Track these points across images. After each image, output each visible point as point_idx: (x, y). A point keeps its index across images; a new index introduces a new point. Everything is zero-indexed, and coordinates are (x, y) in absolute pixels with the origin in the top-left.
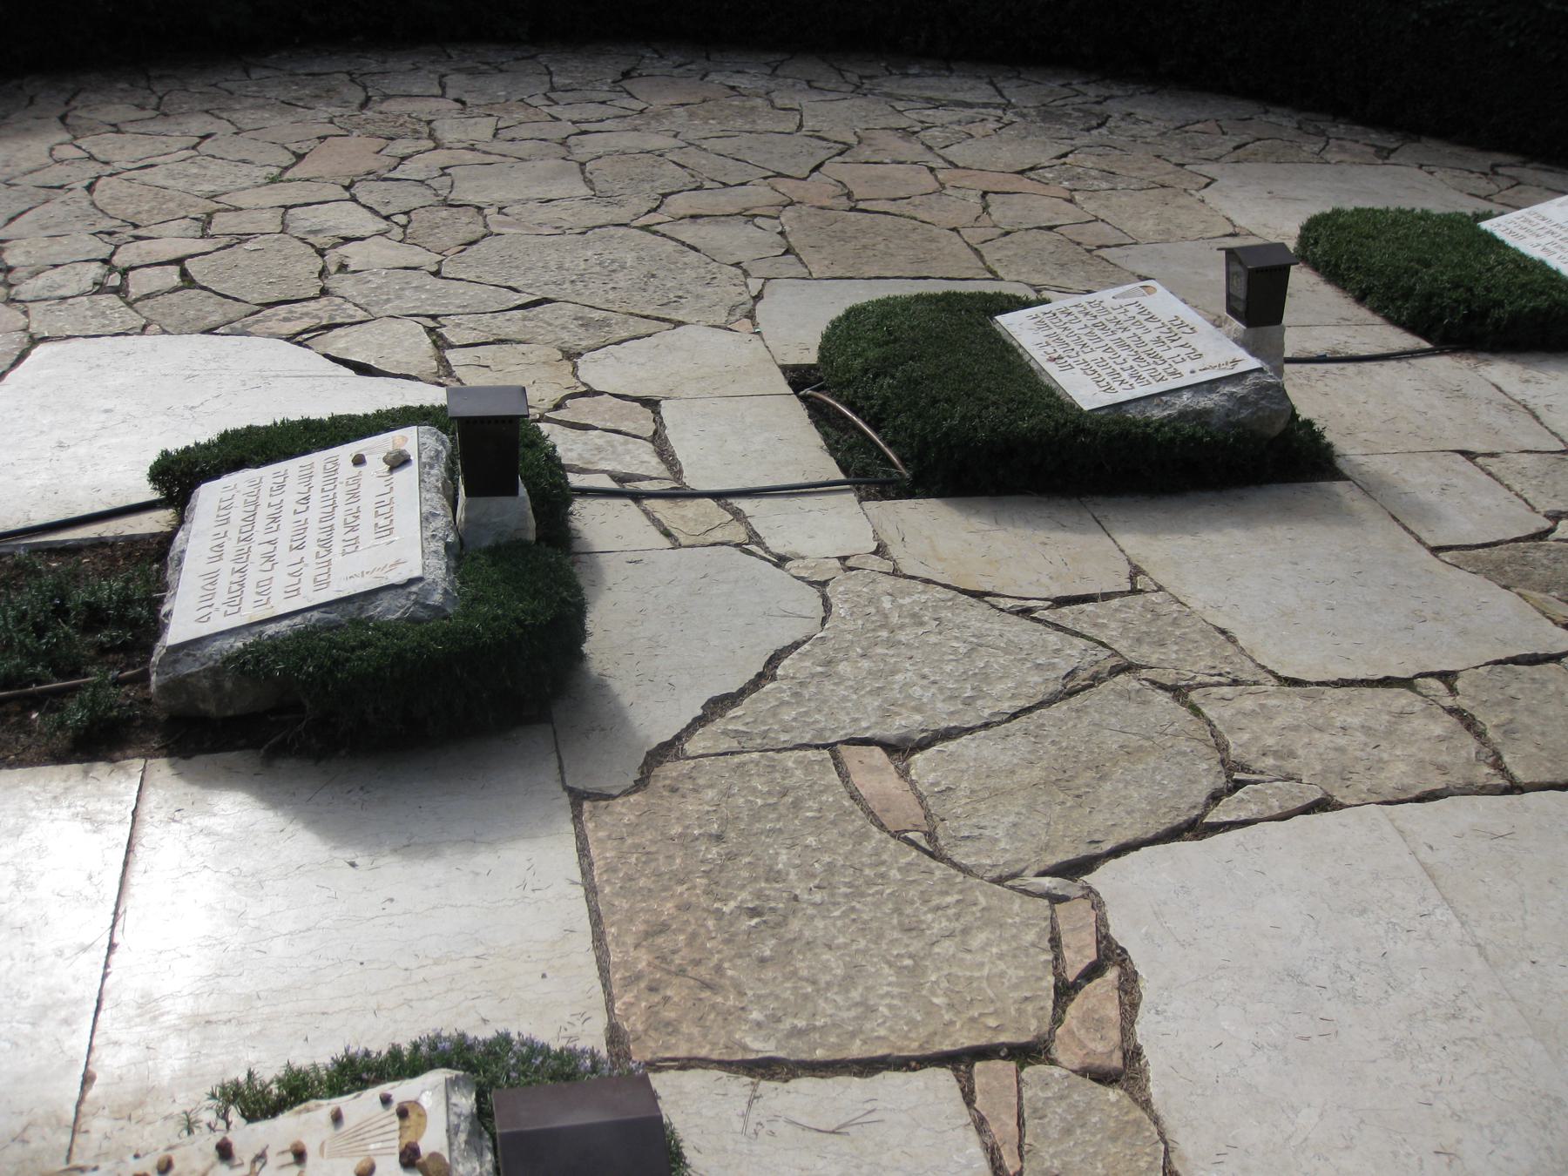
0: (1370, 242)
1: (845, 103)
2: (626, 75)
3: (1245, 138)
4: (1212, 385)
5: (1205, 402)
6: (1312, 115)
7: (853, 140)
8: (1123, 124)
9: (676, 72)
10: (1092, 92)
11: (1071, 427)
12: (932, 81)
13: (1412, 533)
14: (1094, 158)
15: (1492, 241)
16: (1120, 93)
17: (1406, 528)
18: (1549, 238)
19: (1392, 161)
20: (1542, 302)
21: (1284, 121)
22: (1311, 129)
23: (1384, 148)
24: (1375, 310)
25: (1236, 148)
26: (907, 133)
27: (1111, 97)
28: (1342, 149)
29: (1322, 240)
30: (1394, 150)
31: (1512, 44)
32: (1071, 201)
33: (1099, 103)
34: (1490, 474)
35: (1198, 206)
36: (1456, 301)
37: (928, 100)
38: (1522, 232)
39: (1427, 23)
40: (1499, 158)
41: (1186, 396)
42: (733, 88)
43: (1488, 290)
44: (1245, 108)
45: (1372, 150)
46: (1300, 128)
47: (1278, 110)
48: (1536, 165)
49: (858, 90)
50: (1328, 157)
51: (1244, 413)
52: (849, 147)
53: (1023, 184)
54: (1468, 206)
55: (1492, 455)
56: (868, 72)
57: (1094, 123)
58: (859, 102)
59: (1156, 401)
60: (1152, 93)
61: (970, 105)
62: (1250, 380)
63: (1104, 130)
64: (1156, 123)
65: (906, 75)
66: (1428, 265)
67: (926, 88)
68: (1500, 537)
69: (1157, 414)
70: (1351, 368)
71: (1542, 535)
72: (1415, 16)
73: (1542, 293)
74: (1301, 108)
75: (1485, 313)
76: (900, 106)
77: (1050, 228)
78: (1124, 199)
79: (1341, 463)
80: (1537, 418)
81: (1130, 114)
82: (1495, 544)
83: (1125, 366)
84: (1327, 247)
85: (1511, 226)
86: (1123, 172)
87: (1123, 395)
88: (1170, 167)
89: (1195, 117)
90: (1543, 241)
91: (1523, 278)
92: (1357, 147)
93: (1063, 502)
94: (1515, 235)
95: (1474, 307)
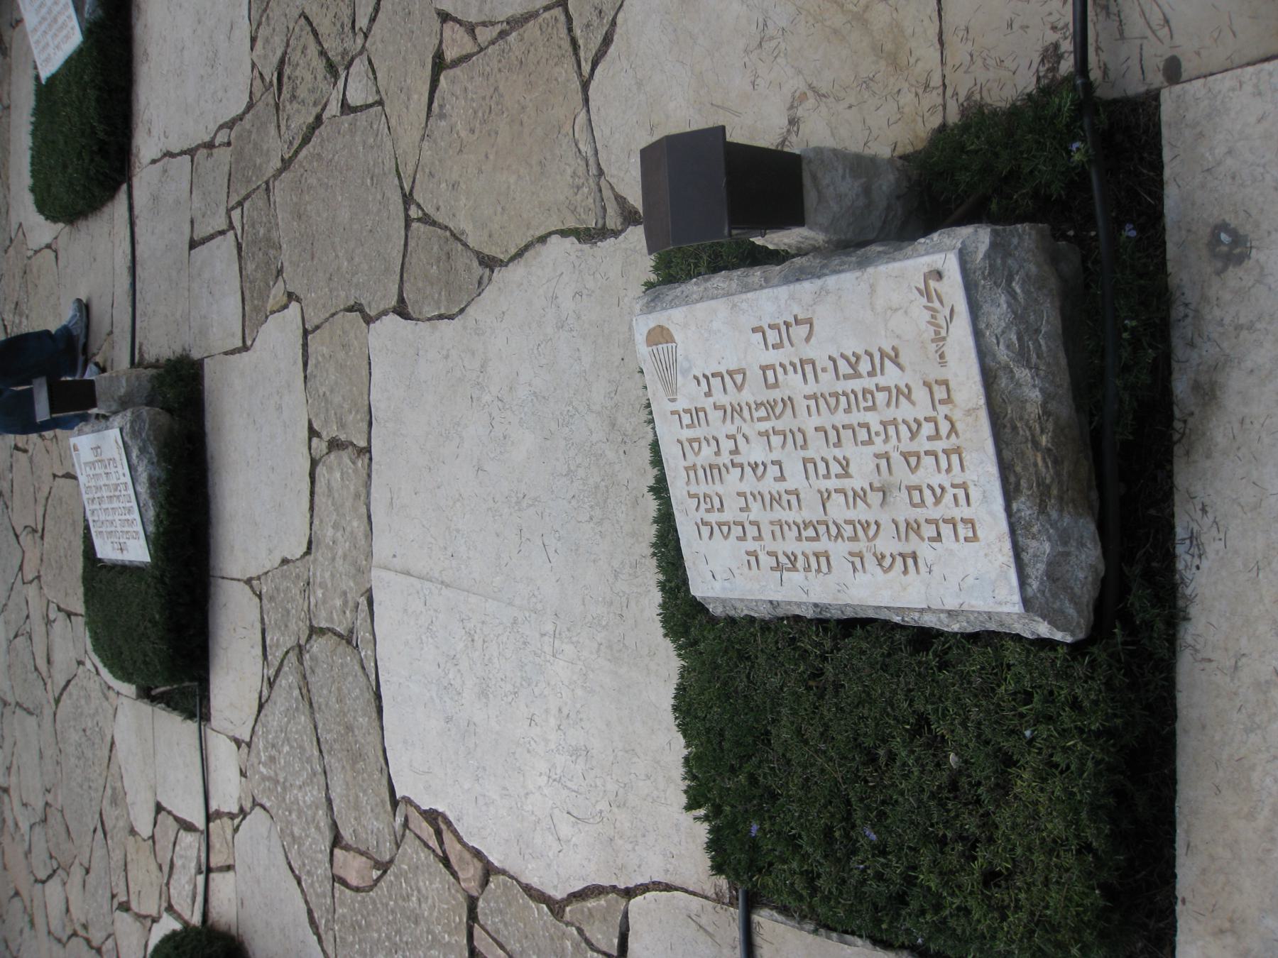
20: (92, 93)
62: (130, 442)
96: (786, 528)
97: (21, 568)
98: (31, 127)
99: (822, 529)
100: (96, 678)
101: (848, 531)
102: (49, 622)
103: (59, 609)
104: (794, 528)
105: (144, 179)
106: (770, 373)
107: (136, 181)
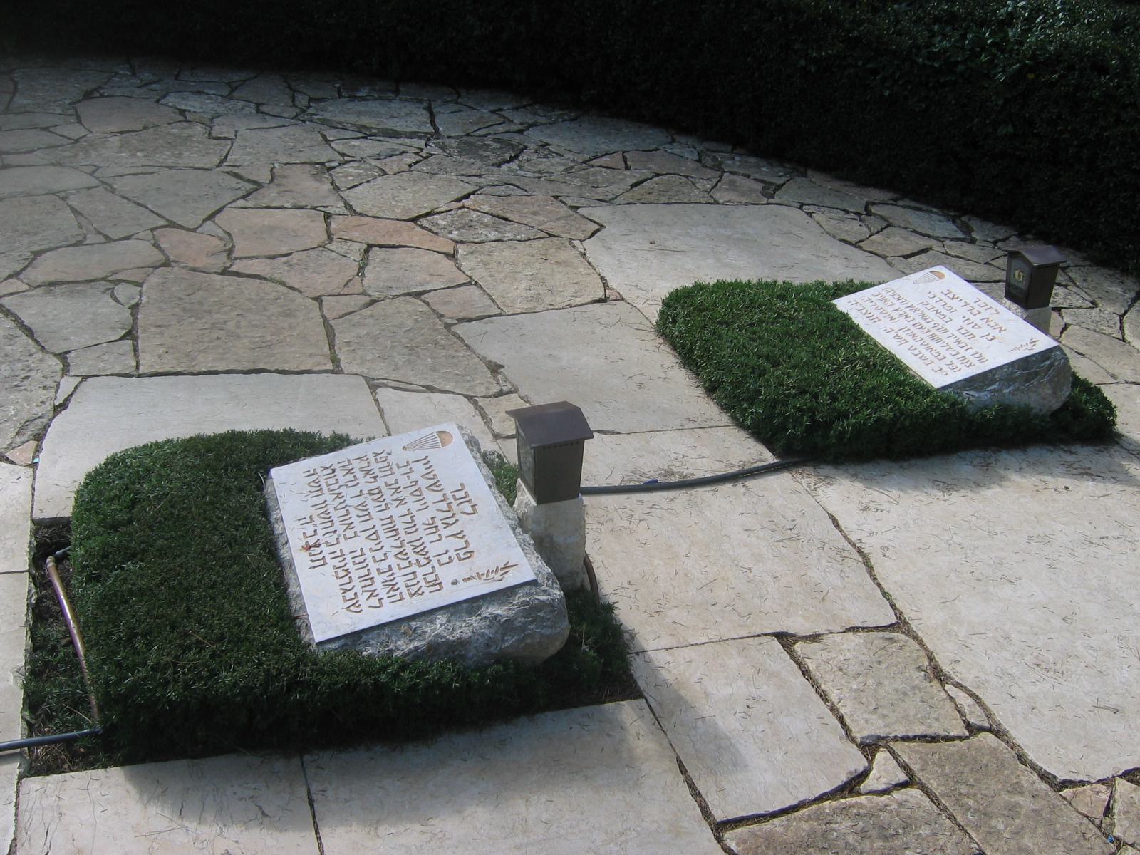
0: (723, 330)
1: (280, 132)
2: (88, 96)
3: (647, 173)
4: (472, 605)
5: (465, 628)
6: (713, 146)
7: (264, 177)
8: (535, 157)
9: (138, 91)
10: (518, 118)
11: (284, 680)
12: (374, 106)
13: (696, 794)
14: (493, 200)
15: (846, 325)
16: (543, 120)
17: (691, 785)
18: (902, 323)
19: (776, 200)
20: (886, 412)
21: (686, 151)
22: (709, 162)
23: (771, 183)
24: (725, 407)
25: (633, 186)
26: (324, 169)
27: (534, 125)
28: (733, 186)
29: (680, 321)
30: (780, 187)
31: (887, 93)
32: (452, 256)
33: (520, 132)
34: (806, 673)
35: (578, 261)
36: (800, 410)
37: (361, 128)
38: (876, 313)
39: (813, 69)
40: (876, 195)
41: (441, 619)
42: (182, 112)
43: (834, 398)
44: (654, 136)
45: (759, 186)
46: (699, 161)
47: (683, 139)
48: (906, 202)
49: (301, 117)
50: (717, 195)
51: (510, 641)
52: (259, 185)
53: (416, 235)
54: (834, 269)
55: (814, 638)
56: (320, 94)
57: (507, 156)
58: (296, 130)
59: (403, 628)
60: (572, 120)
61: (395, 134)
62: (518, 599)
63: (514, 165)
64: (567, 156)
65: (353, 98)
66: (776, 364)
67: (365, 113)
68: (803, 795)
69: (403, 646)
70: (681, 496)
71: (851, 786)
72: (803, 63)
73: (888, 401)
74: (705, 139)
75: (828, 425)
76: (331, 134)
77: (418, 295)
78: (507, 253)
79: (639, 671)
80: (870, 568)
81: (544, 145)
82: (794, 809)
83: (384, 566)
84: (683, 329)
85: (867, 305)
86: (516, 217)
87: (367, 619)
88: (564, 210)
89: (604, 148)
90: (896, 326)
91: (870, 382)
92: (747, 183)
93: (279, 765)
94: (871, 317)
95: (818, 417)
96: (341, 559)
97: (172, 225)
98: (744, 280)
99: (347, 579)
100: (48, 407)
101: (350, 595)
102: (111, 282)
103: (135, 308)
104: (343, 564)
105: (790, 492)
106: (377, 491)
107: (783, 480)
